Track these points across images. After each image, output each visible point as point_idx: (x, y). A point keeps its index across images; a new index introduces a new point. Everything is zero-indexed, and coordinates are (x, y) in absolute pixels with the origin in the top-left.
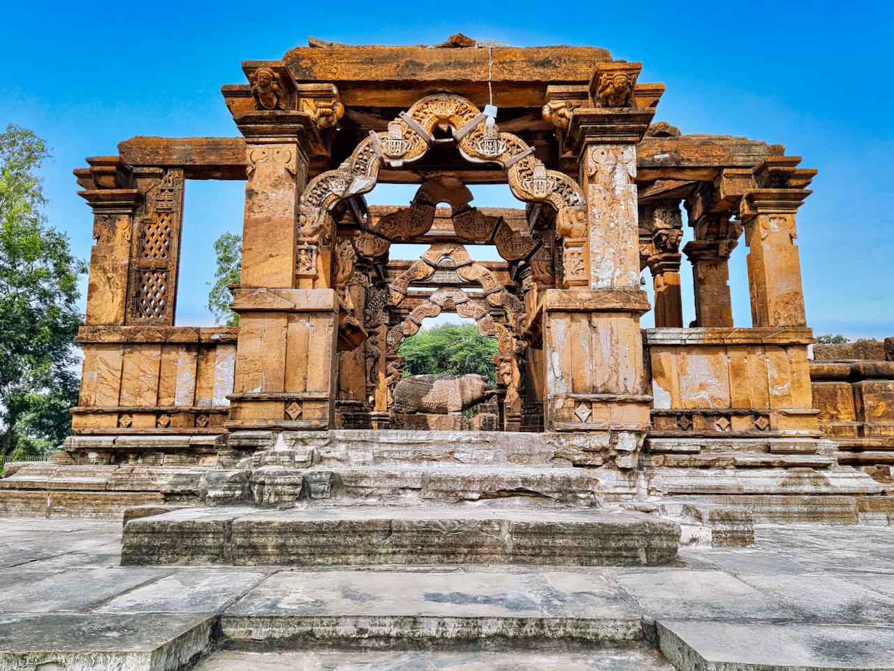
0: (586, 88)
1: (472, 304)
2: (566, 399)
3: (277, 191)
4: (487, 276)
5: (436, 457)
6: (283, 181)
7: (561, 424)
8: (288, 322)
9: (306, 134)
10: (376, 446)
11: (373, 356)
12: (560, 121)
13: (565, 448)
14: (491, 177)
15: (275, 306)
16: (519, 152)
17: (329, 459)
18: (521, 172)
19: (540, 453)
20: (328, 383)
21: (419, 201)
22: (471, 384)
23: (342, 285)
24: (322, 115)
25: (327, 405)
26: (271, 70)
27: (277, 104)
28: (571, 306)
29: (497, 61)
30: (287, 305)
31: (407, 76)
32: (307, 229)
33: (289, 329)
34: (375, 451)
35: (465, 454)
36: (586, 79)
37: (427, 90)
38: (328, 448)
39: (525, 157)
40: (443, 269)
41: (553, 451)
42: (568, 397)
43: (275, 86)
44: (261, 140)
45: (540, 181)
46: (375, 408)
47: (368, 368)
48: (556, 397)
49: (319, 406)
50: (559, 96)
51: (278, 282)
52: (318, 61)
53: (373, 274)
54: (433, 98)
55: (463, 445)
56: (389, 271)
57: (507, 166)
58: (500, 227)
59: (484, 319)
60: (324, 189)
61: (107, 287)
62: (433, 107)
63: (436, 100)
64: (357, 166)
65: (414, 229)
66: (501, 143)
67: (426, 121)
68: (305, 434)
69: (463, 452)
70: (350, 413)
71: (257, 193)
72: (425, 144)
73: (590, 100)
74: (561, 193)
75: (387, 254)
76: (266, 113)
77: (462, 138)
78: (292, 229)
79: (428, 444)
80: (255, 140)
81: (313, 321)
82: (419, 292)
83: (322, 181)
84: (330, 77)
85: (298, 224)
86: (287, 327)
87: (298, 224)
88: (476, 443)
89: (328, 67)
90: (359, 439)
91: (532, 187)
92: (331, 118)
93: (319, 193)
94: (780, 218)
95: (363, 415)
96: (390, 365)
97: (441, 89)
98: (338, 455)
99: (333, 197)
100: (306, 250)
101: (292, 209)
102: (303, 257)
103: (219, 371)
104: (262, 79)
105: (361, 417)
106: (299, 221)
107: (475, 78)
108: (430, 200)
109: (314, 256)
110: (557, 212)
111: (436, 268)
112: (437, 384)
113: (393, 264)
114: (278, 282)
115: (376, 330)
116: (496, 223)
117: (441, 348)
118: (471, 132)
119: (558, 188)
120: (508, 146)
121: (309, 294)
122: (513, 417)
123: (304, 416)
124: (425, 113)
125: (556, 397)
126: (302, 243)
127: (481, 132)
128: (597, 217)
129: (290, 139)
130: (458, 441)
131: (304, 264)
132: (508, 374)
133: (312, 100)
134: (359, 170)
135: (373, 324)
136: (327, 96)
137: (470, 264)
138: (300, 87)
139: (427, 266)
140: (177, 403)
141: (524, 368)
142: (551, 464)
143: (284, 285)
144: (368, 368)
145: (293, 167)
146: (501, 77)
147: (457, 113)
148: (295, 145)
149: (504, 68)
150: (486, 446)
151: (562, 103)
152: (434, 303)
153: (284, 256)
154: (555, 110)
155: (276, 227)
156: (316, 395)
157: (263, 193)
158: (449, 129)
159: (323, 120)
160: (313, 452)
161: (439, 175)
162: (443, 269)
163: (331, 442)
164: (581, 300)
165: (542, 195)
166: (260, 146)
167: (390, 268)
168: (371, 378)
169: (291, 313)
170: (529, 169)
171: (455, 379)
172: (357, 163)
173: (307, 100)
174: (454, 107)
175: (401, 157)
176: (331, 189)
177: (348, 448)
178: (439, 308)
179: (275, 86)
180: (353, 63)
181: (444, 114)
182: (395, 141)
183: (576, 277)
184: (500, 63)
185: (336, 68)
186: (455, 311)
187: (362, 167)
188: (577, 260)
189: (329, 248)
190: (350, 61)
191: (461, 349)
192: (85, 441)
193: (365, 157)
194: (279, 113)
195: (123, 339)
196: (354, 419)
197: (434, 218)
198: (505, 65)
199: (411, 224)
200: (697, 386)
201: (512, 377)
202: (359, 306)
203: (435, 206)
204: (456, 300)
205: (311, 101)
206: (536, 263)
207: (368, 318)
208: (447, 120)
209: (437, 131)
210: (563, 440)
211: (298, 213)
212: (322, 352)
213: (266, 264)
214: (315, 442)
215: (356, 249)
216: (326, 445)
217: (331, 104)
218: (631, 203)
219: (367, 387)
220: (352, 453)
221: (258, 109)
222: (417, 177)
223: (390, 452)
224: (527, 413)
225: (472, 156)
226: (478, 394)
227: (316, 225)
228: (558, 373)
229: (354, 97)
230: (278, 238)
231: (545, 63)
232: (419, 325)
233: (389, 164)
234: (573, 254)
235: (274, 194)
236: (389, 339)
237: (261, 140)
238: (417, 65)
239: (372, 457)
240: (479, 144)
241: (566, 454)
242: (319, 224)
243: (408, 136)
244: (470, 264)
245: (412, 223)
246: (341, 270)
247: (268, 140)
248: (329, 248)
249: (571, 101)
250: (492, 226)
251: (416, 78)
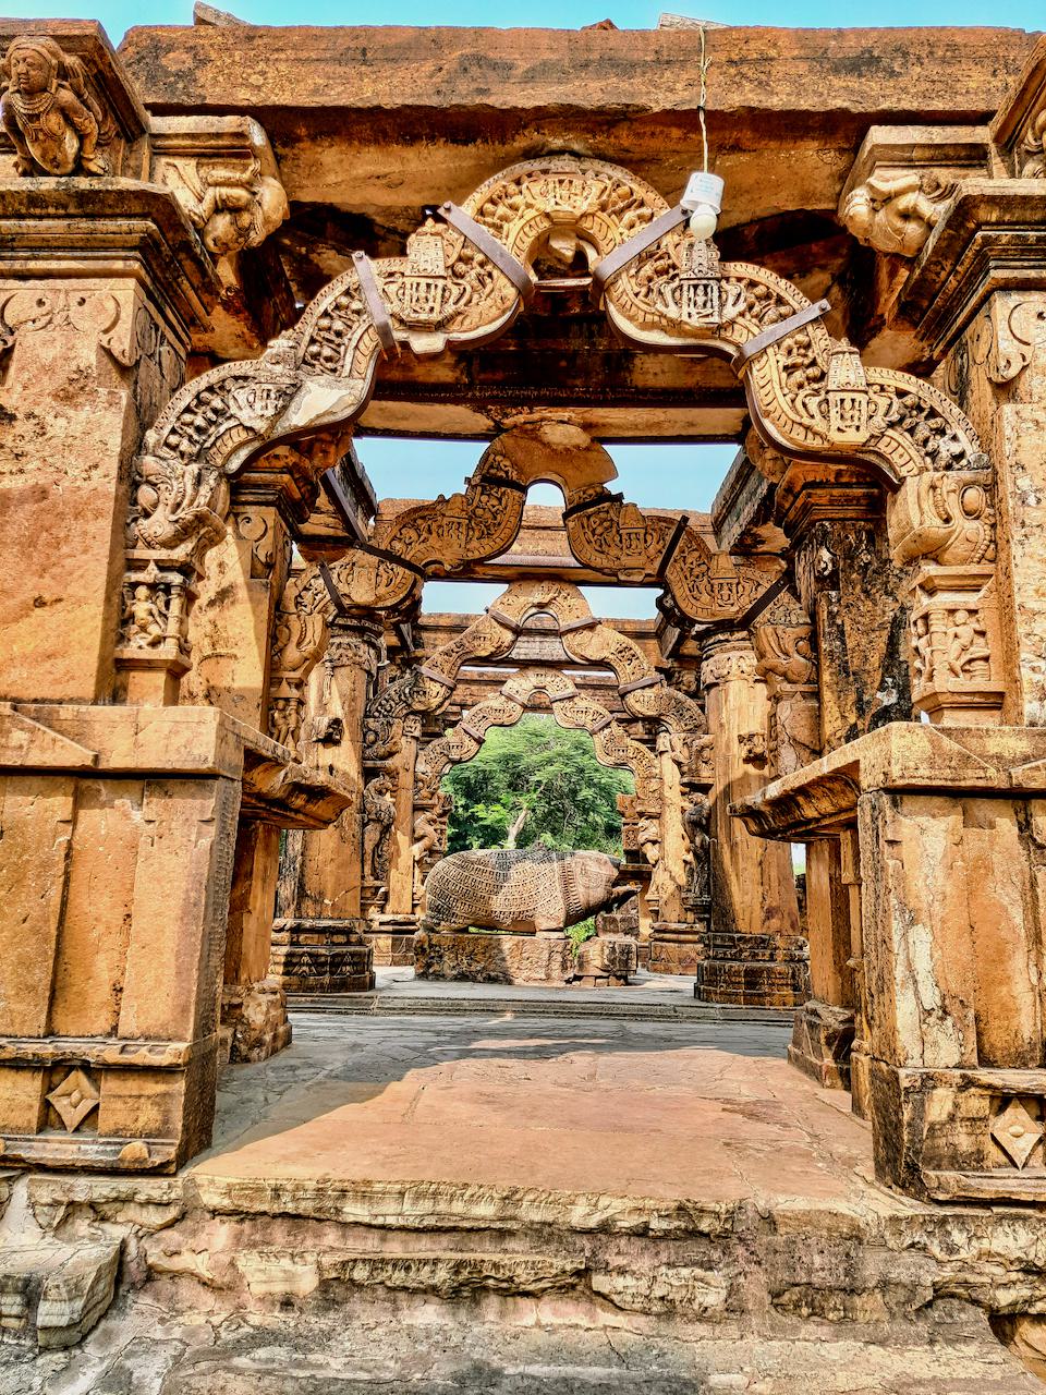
0: (983, 135)
1: (586, 701)
2: (962, 1088)
3: (71, 413)
4: (627, 654)
5: (531, 1288)
6: (92, 385)
7: (950, 1176)
8: (77, 805)
9: (168, 255)
10: (331, 1237)
11: (378, 820)
12: (899, 231)
13: (964, 1266)
14: (658, 424)
15: (34, 759)
16: (783, 317)
17: (175, 1275)
18: (790, 369)
19: (885, 1285)
20: (185, 1010)
21: (488, 479)
22: (584, 872)
23: (297, 675)
24: (221, 207)
25: (180, 1086)
26: (52, 43)
27: (79, 159)
28: (970, 779)
29: (723, 57)
30: (73, 755)
31: (463, 95)
32: (160, 524)
33: (81, 827)
34: (327, 1260)
35: (629, 1281)
36: (982, 107)
37: (521, 143)
38: (173, 1237)
39: (802, 329)
40: (530, 632)
41: (928, 1280)
42: (968, 1083)
43: (67, 96)
44: (32, 265)
45: (848, 396)
46: (388, 908)
47: (369, 846)
48: (929, 1081)
49: (154, 1087)
50: (904, 158)
51: (57, 682)
52: (213, 55)
53: (388, 640)
54: (537, 165)
55: (623, 1242)
56: (425, 635)
57: (749, 351)
58: (681, 543)
59: (607, 731)
60: (215, 411)
62: (537, 188)
63: (545, 172)
64: (314, 349)
65: (475, 543)
66: (732, 289)
67: (513, 228)
68: (103, 1188)
69: (622, 1271)
70: (322, 951)
71: (12, 418)
72: (511, 292)
73: (996, 162)
74: (911, 431)
75: (417, 603)
76: (47, 184)
77: (617, 275)
78: (105, 526)
79: (503, 1234)
80: (17, 265)
81: (155, 805)
82: (482, 674)
83: (210, 389)
84: (243, 97)
85: (129, 507)
86: (73, 821)
87: (129, 507)
88: (666, 1236)
89: (238, 70)
90: (276, 1208)
91: (825, 416)
92: (245, 219)
93: (200, 421)
95: (353, 955)
96: (421, 818)
97: (557, 143)
98: (201, 1265)
99: (240, 436)
100: (153, 587)
101: (112, 466)
102: (141, 608)
104: (22, 68)
105: (348, 959)
106: (135, 502)
107: (659, 101)
108: (514, 475)
109: (176, 604)
110: (896, 489)
111: (518, 632)
112: (516, 873)
113: (431, 622)
114: (57, 682)
115: (388, 763)
116: (672, 532)
117: (516, 757)
118: (643, 257)
119: (902, 419)
120: (752, 299)
121: (142, 720)
122: (665, 931)
123: (106, 1121)
124: (514, 208)
125: (929, 1081)
126: (141, 565)
127: (674, 259)
128: (1032, 500)
129: (119, 265)
130: (605, 1228)
131: (143, 629)
132: (654, 842)
133: (193, 162)
134: (321, 359)
135: (382, 751)
136: (238, 151)
137: (591, 627)
138: (158, 124)
139: (499, 629)
141: (707, 852)
142: (922, 1327)
143: (71, 690)
144: (369, 846)
145: (122, 342)
146: (735, 100)
147: (603, 208)
148: (131, 283)
149: (744, 76)
150: (696, 1250)
151: (910, 177)
152: (510, 698)
153: (79, 603)
154: (888, 199)
155: (61, 516)
156: (143, 1055)
157: (30, 416)
158: (580, 257)
159: (222, 224)
160: (123, 1249)
161: (536, 416)
162: (530, 632)
163: (183, 1217)
164: (999, 757)
165: (854, 437)
166: (31, 283)
167: (425, 628)
168: (374, 869)
169: (85, 781)
170: (813, 363)
171: (550, 860)
172: (313, 341)
173: (178, 162)
174: (595, 191)
175: (440, 326)
176: (233, 410)
177: (238, 1238)
178: (519, 709)
179: (67, 96)
180: (308, 60)
181: (565, 207)
182: (423, 282)
183: (964, 684)
184: (731, 62)
185: (263, 73)
186: (548, 709)
187: (327, 352)
188: (966, 633)
189: (265, 586)
190: (304, 55)
191: (550, 762)
193: (338, 325)
194: (83, 183)
196: (332, 964)
197: (520, 527)
198: (745, 69)
199: (473, 535)
201: (662, 849)
202: (352, 712)
203: (524, 490)
204: (553, 693)
205: (188, 166)
206: (770, 629)
207: (371, 737)
208: (575, 228)
209: (542, 259)
210: (958, 1237)
211: (131, 478)
212: (174, 906)
213: (24, 625)
214: (132, 1212)
215: (332, 589)
216: (169, 1226)
217: (246, 176)
219: (363, 888)
220: (249, 1263)
221: (24, 174)
222: (482, 422)
223: (377, 1264)
224: (715, 958)
225: (645, 326)
226: (598, 894)
227: (186, 514)
228: (931, 998)
229: (316, 167)
230: (65, 549)
231: (863, 63)
232: (480, 742)
233: (405, 345)
234: (952, 612)
235: (62, 422)
236: (421, 768)
237: (32, 265)
238: (494, 66)
239: (315, 1283)
240: (667, 291)
241: (965, 1284)
242: (193, 509)
243: (461, 267)
244: (591, 627)
245: (469, 528)
246: (295, 639)
247: (54, 265)
248: (265, 586)
249: (936, 171)
250: (662, 538)
251: (490, 101)
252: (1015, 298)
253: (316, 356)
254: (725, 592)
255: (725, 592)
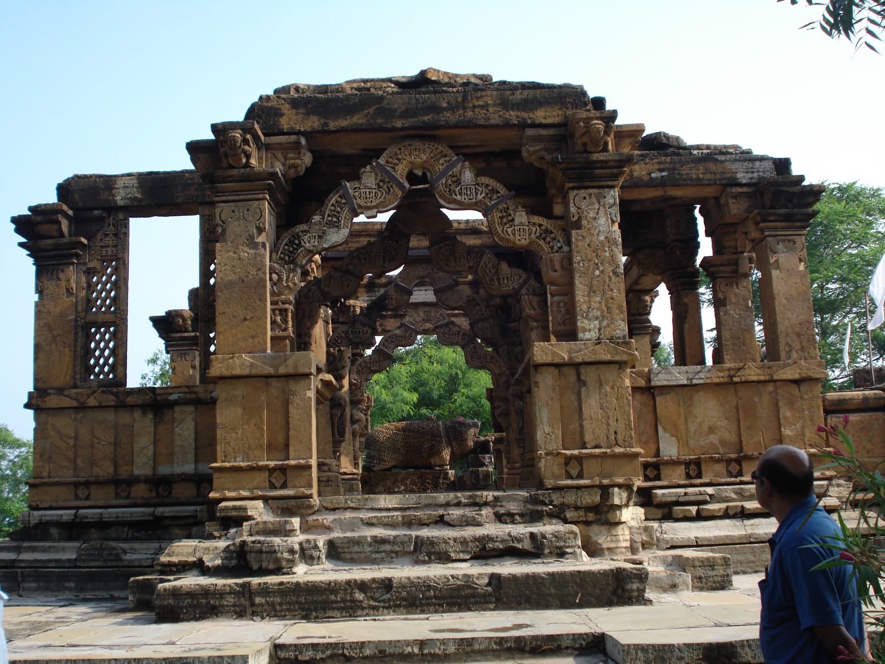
61: (53, 346)
63: (410, 145)
91: (514, 235)
94: (789, 241)
103: (179, 435)
124: (399, 160)
140: (136, 472)
182: (367, 191)
187: (335, 219)
192: (45, 516)
195: (74, 404)
200: (706, 429)
209: (411, 177)
218: (615, 249)
252: (576, 192)
253: (331, 221)
254: (506, 281)
255: (506, 281)
